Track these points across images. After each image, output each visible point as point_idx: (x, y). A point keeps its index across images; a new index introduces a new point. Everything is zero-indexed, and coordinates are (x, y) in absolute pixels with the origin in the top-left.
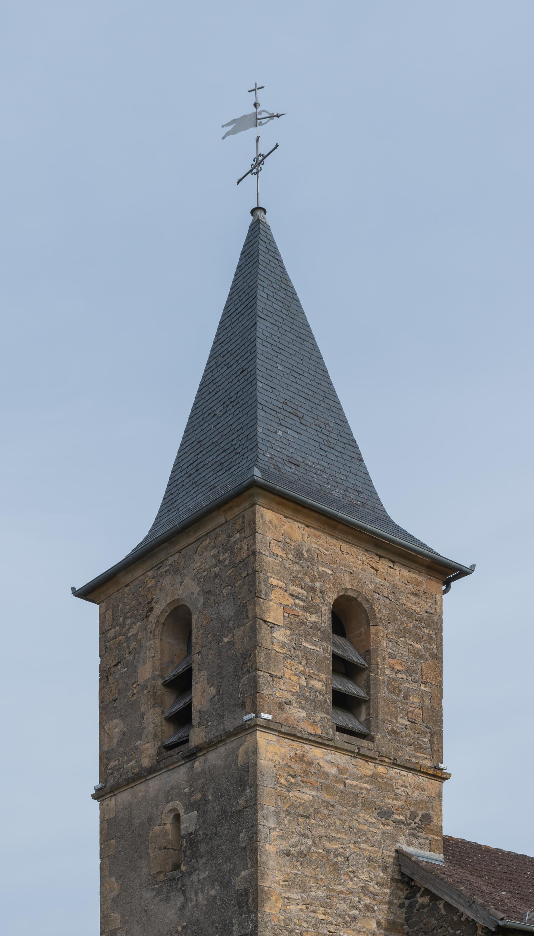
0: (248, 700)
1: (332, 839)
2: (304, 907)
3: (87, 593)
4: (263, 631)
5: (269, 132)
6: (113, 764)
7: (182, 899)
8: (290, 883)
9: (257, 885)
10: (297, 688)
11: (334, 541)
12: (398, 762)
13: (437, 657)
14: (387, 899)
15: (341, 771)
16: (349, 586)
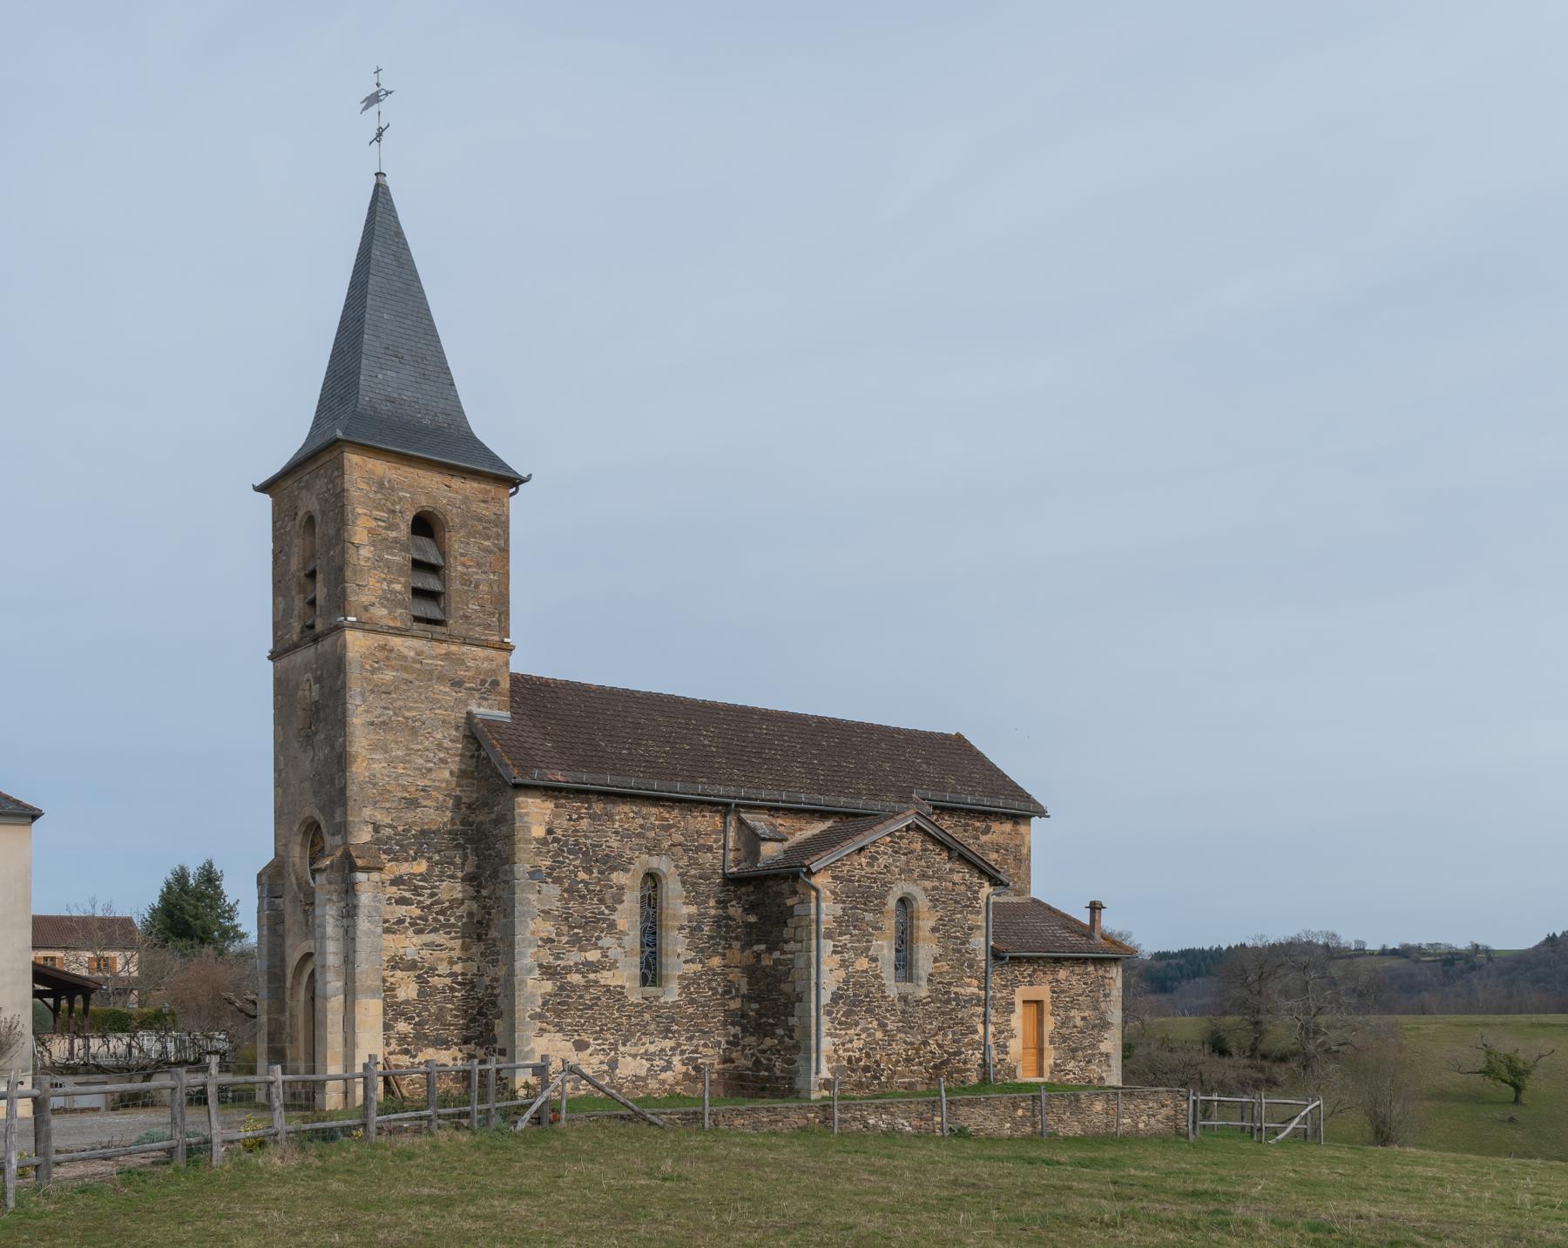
1: (410, 709)
3: (264, 488)
5: (386, 104)
8: (374, 747)
13: (505, 551)
15: (418, 654)
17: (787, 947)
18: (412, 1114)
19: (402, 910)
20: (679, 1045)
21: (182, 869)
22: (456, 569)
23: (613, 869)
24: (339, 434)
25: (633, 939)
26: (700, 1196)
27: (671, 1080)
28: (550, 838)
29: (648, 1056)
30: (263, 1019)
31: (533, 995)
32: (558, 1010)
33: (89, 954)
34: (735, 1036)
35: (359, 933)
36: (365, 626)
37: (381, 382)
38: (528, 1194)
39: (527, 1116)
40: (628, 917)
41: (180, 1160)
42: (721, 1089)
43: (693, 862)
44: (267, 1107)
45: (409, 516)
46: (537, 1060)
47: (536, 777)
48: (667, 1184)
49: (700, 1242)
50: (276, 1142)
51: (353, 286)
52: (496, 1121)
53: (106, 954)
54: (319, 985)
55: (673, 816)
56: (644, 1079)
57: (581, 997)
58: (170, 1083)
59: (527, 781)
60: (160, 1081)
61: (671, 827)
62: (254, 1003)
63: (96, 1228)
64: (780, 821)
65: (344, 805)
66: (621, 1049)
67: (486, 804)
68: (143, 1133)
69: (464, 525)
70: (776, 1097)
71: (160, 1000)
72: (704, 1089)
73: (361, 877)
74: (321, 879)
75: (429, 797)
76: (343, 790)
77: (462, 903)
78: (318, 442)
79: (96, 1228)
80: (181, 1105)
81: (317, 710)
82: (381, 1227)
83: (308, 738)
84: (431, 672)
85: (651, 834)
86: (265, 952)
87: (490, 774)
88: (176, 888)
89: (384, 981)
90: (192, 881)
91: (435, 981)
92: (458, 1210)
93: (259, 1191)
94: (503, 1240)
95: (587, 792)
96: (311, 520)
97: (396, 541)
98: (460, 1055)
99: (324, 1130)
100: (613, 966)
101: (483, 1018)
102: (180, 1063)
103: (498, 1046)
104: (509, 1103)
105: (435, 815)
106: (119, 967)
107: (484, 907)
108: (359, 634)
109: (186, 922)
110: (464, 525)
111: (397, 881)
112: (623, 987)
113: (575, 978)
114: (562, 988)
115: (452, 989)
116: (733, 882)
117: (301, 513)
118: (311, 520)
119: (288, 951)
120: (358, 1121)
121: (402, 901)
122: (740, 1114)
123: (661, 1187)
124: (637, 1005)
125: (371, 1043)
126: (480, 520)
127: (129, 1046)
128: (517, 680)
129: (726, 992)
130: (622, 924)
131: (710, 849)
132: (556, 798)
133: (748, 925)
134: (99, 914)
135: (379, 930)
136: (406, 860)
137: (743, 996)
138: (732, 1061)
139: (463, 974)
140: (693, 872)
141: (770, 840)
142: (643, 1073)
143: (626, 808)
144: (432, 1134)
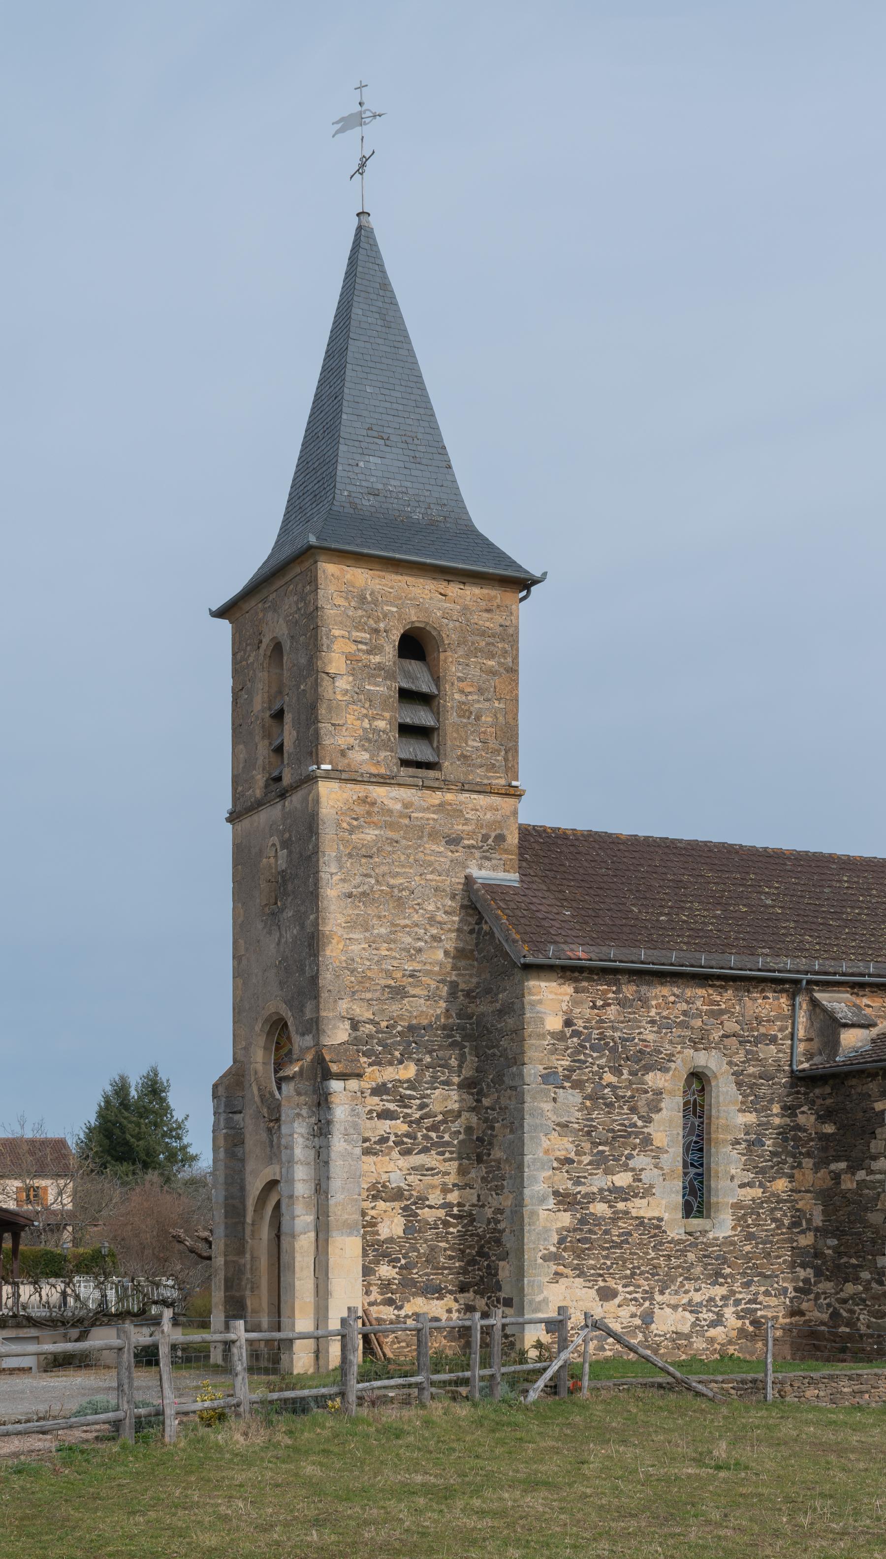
0: (314, 750)
1: (396, 875)
2: (366, 946)
3: (222, 613)
4: (325, 683)
5: (371, 129)
6: (240, 789)
7: (278, 934)
8: (352, 925)
9: (318, 930)
10: (361, 732)
11: (399, 577)
12: (466, 787)
13: (513, 670)
14: (456, 926)
15: (406, 806)
16: (415, 619)
17: (876, 1165)
18: (400, 1381)
19: (385, 1126)
20: (733, 1293)
21: (123, 1079)
22: (453, 697)
23: (648, 1069)
24: (313, 540)
25: (673, 1156)
26: (765, 1491)
27: (722, 1338)
28: (568, 1031)
29: (692, 1307)
30: (219, 1261)
31: (547, 1230)
32: (580, 1248)
33: (18, 1183)
34: (806, 1281)
35: (333, 1155)
36: (346, 776)
37: (367, 472)
38: (546, 1484)
39: (541, 1384)
40: (667, 1129)
41: (128, 1435)
42: (787, 1351)
43: (752, 1058)
44: (226, 1369)
45: (396, 636)
46: (551, 1313)
47: (551, 954)
48: (722, 1474)
49: (768, 1552)
50: (238, 1415)
51: (329, 355)
52: (502, 1389)
53: (37, 1183)
54: (285, 1220)
55: (726, 998)
56: (688, 1337)
57: (606, 1232)
58: (116, 1342)
59: (541, 960)
60: (102, 1338)
61: (722, 1012)
62: (210, 1244)
63: (34, 1517)
64: (866, 1001)
65: (316, 997)
66: (658, 1298)
67: (488, 991)
68: (84, 1401)
69: (462, 642)
70: (861, 1360)
71: (98, 1238)
72: (767, 1351)
73: (336, 1085)
74: (288, 1089)
75: (418, 984)
76: (314, 979)
77: (459, 1115)
78: (288, 551)
79: (34, 1517)
80: (128, 1369)
81: (285, 881)
82: (367, 1523)
83: (273, 916)
84: (422, 828)
85: (697, 1023)
86: (221, 1179)
87: (493, 949)
88: (115, 1102)
89: (364, 1214)
90: (133, 1093)
91: (426, 1214)
92: (460, 1504)
93: (221, 1474)
94: (518, 1543)
95: (615, 971)
96: (278, 648)
97: (379, 667)
98: (455, 1306)
99: (294, 1400)
100: (648, 1192)
101: (485, 1260)
102: (123, 1315)
103: (502, 1295)
104: (518, 1367)
105: (426, 1007)
106: (51, 1198)
107: (486, 1120)
108: (334, 785)
109: (127, 1143)
110: (462, 642)
111: (379, 1090)
112: (660, 1219)
113: (600, 1208)
114: (583, 1221)
115: (446, 1224)
116: (804, 1081)
117: (266, 641)
118: (278, 648)
119: (249, 1178)
120: (334, 1390)
121: (385, 1115)
122: (813, 1382)
123: (714, 1478)
124: (679, 1242)
125: (347, 1293)
126: (483, 634)
127: (64, 1294)
128: (527, 834)
129: (795, 1224)
130: (660, 1138)
131: (773, 1040)
132: (576, 980)
133: (823, 1137)
134: (29, 1135)
135: (358, 1151)
136: (391, 1064)
137: (817, 1229)
138: (801, 1313)
139: (459, 1205)
140: (751, 1070)
141: (853, 1026)
142: (686, 1329)
143: (665, 991)
144: (423, 1406)
